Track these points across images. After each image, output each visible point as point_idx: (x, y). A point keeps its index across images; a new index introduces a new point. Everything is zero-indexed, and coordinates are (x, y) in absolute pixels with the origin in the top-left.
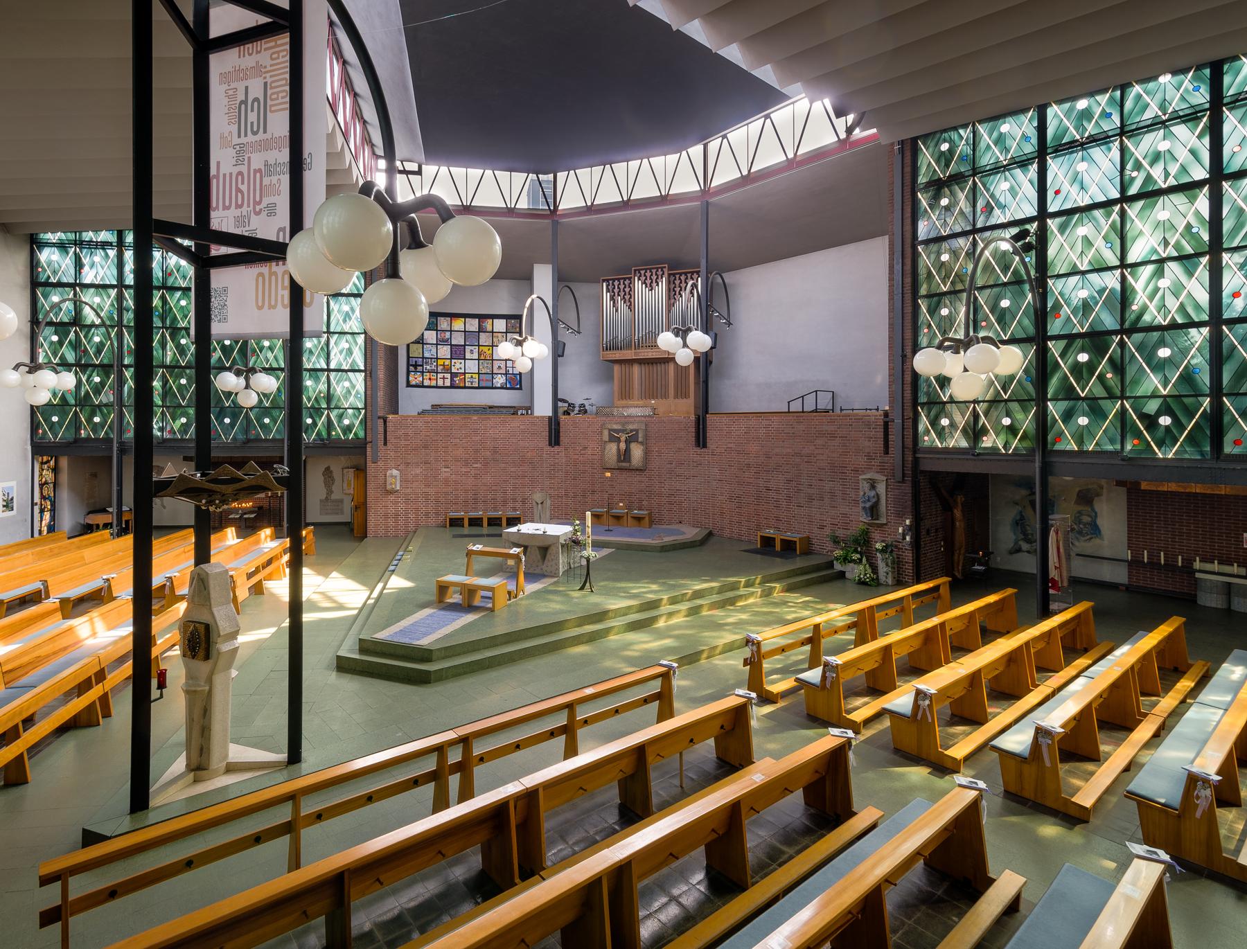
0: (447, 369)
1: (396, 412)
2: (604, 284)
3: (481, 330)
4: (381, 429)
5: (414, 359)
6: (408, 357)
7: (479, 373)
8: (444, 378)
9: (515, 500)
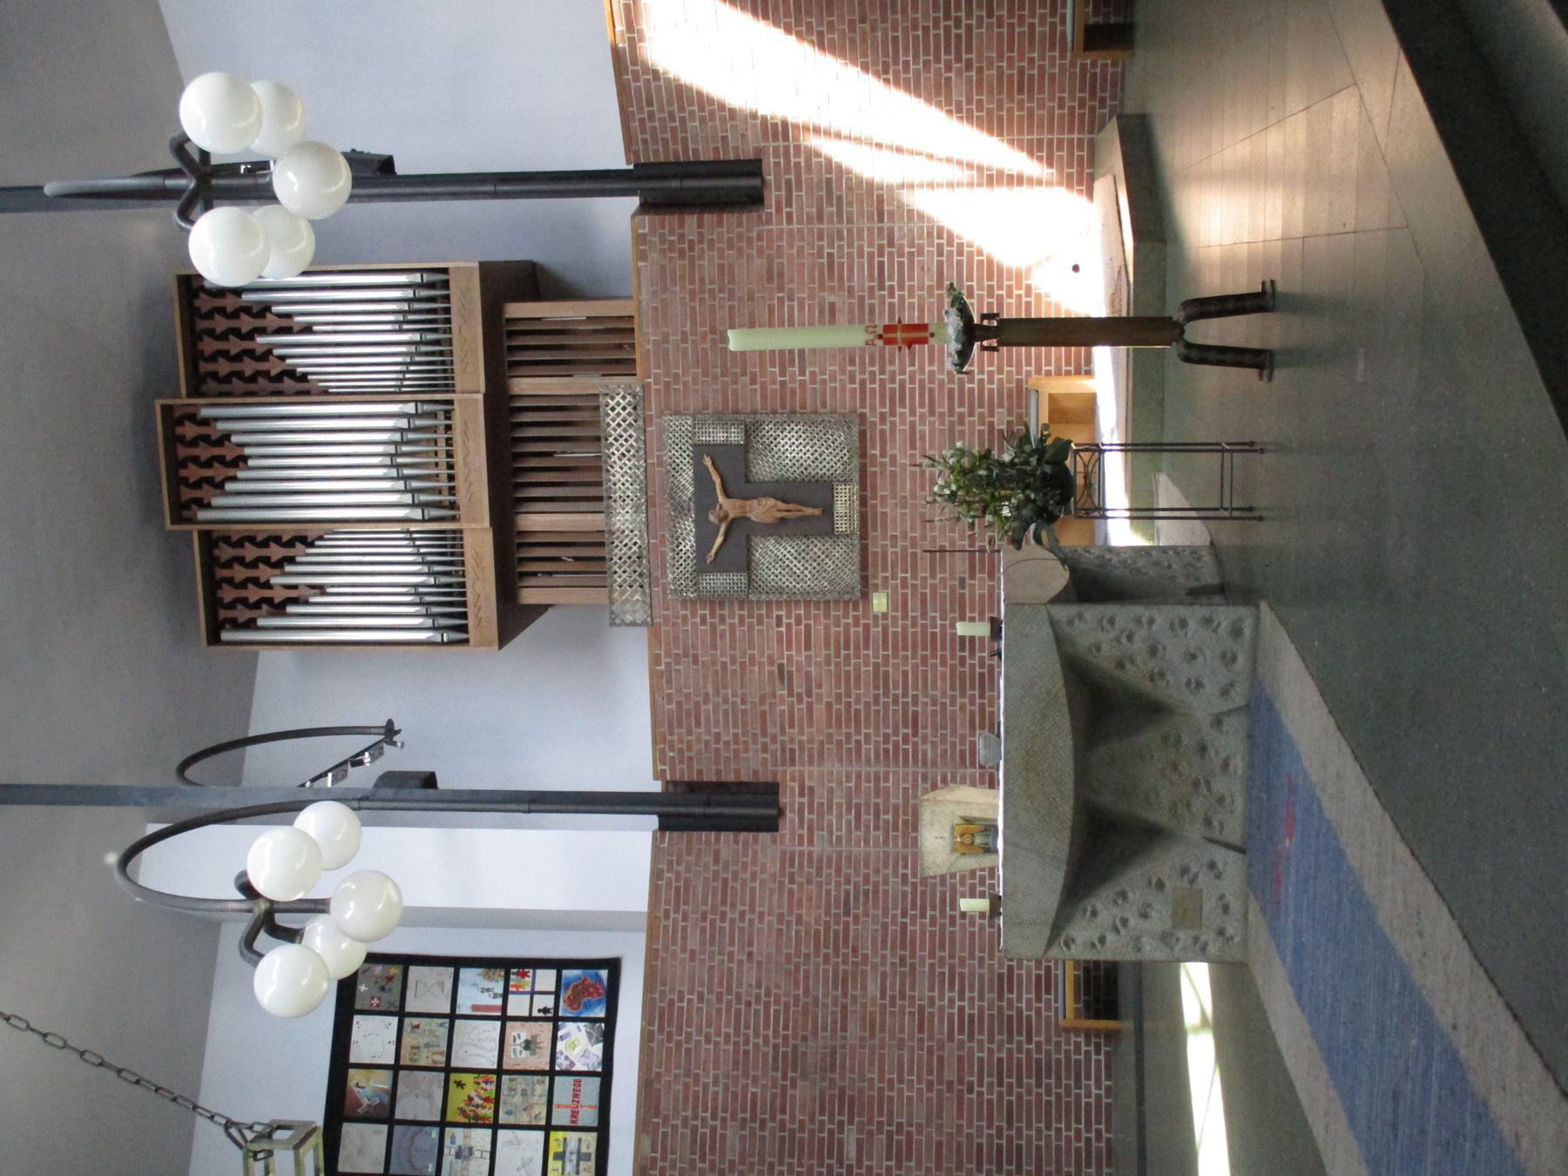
3: (384, 1114)
7: (548, 1128)
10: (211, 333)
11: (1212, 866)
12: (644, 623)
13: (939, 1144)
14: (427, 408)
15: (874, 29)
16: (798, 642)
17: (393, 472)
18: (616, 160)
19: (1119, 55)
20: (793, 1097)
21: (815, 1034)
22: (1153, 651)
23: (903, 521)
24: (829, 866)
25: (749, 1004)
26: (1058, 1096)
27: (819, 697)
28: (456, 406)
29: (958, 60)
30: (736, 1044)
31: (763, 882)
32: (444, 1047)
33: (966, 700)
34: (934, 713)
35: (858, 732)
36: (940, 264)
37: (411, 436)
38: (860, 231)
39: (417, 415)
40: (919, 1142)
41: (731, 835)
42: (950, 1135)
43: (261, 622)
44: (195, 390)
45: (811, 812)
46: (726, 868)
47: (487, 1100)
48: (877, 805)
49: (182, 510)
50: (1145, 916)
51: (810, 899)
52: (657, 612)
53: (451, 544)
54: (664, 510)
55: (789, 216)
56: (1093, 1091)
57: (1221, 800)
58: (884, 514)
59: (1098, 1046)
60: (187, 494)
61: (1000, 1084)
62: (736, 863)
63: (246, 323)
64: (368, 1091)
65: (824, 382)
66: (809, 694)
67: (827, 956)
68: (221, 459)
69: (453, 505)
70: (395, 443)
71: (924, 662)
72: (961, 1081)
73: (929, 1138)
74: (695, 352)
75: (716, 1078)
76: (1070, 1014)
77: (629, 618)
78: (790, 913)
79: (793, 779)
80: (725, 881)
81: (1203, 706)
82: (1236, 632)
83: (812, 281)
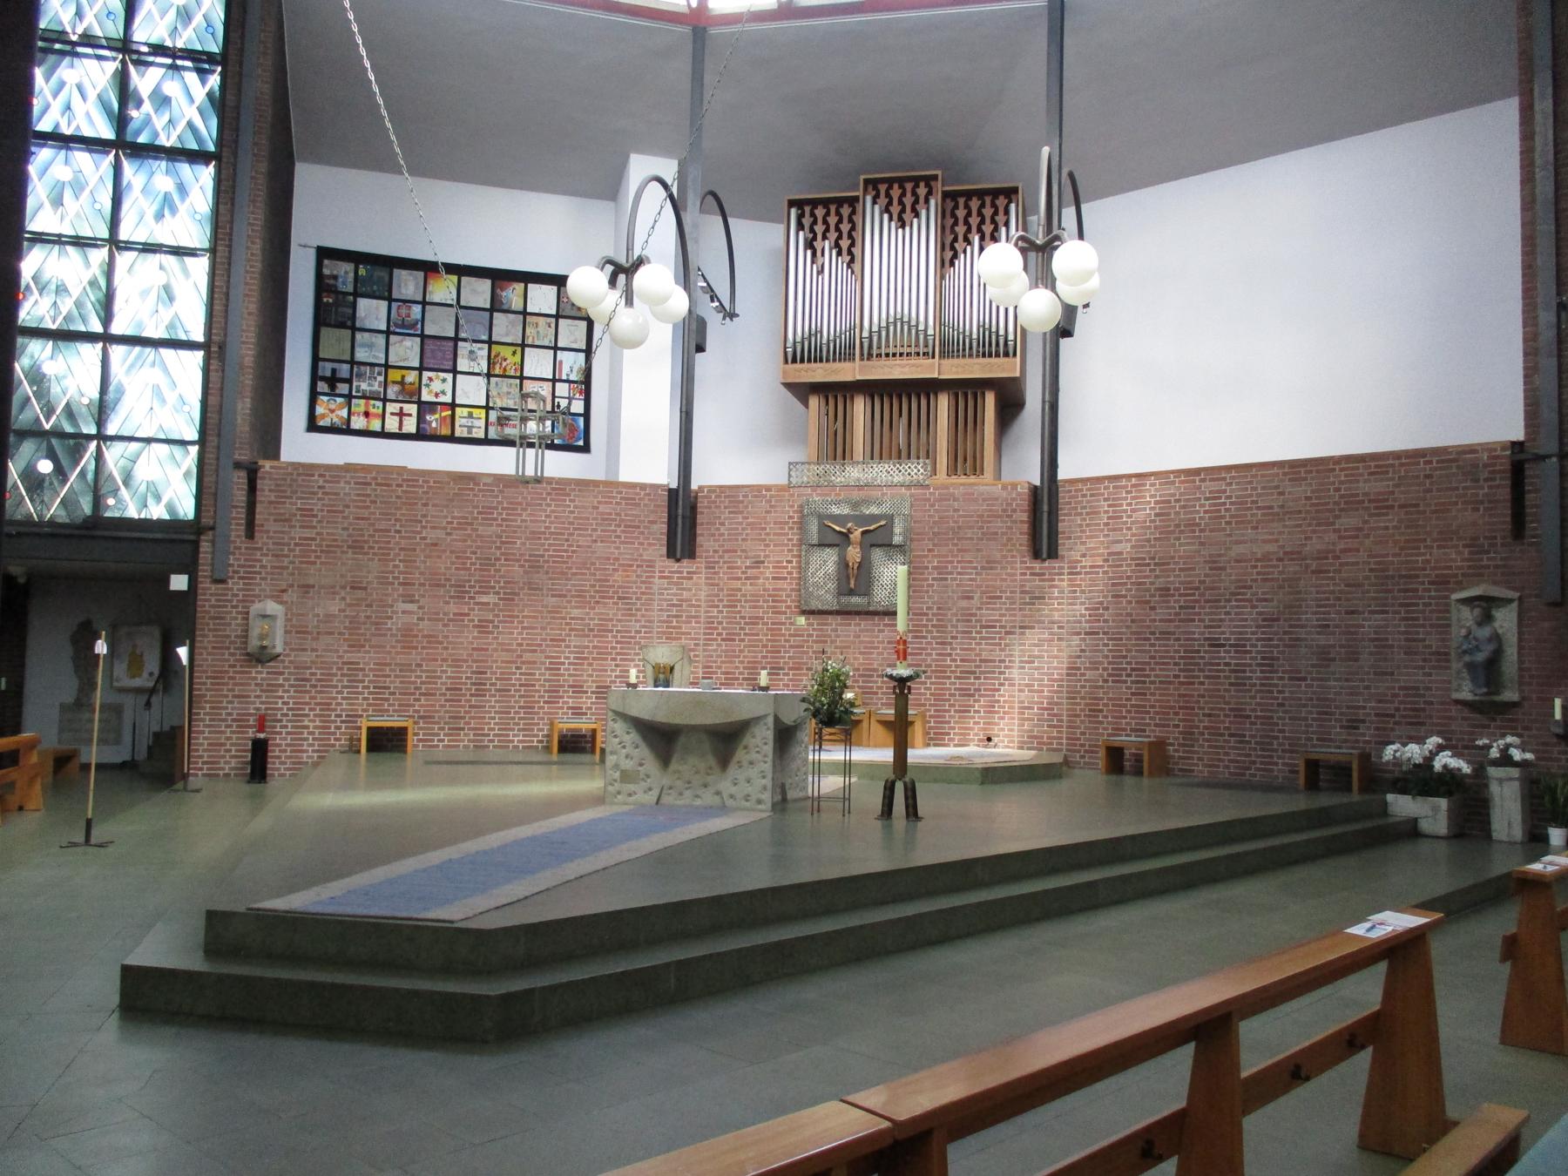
0: (411, 394)
1: (275, 455)
2: (793, 211)
3: (496, 306)
4: (240, 496)
5: (329, 366)
6: (316, 359)
8: (401, 414)
9: (578, 689)
10: (983, 205)
11: (650, 789)
12: (790, 482)
13: (487, 650)
14: (931, 342)
15: (1127, 627)
16: (777, 573)
17: (891, 320)
18: (1062, 474)
19: (1104, 770)
20: (514, 566)
21: (551, 579)
22: (751, 763)
23: (846, 636)
24: (646, 588)
25: (567, 540)
26: (514, 718)
27: (745, 584)
28: (931, 360)
29: (1109, 675)
30: (544, 533)
31: (638, 549)
32: (537, 343)
33: (741, 670)
34: (734, 651)
35: (724, 606)
36: (994, 661)
37: (913, 332)
38: (1015, 615)
39: (926, 335)
40: (488, 638)
41: (665, 531)
42: (492, 656)
43: (801, 233)
44: (946, 195)
45: (678, 578)
46: (645, 527)
47: (505, 370)
48: (681, 616)
49: (872, 184)
50: (627, 757)
51: (628, 576)
52: (796, 490)
53: (845, 353)
54: (856, 495)
55: (1025, 574)
56: (517, 738)
57: (681, 794)
58: (850, 625)
59: (541, 742)
60: (883, 188)
61: (521, 685)
62: (649, 533)
63: (988, 228)
64: (511, 295)
65: (928, 592)
66: (747, 578)
67: (594, 586)
68: (903, 211)
69: (870, 355)
70: (909, 322)
71: (764, 646)
72: (523, 663)
73: (489, 644)
74: (947, 517)
75: (526, 521)
76: (561, 725)
77: (793, 473)
78: (620, 565)
79: (697, 568)
80: (639, 527)
81: (726, 786)
82: (759, 802)
83: (987, 586)
